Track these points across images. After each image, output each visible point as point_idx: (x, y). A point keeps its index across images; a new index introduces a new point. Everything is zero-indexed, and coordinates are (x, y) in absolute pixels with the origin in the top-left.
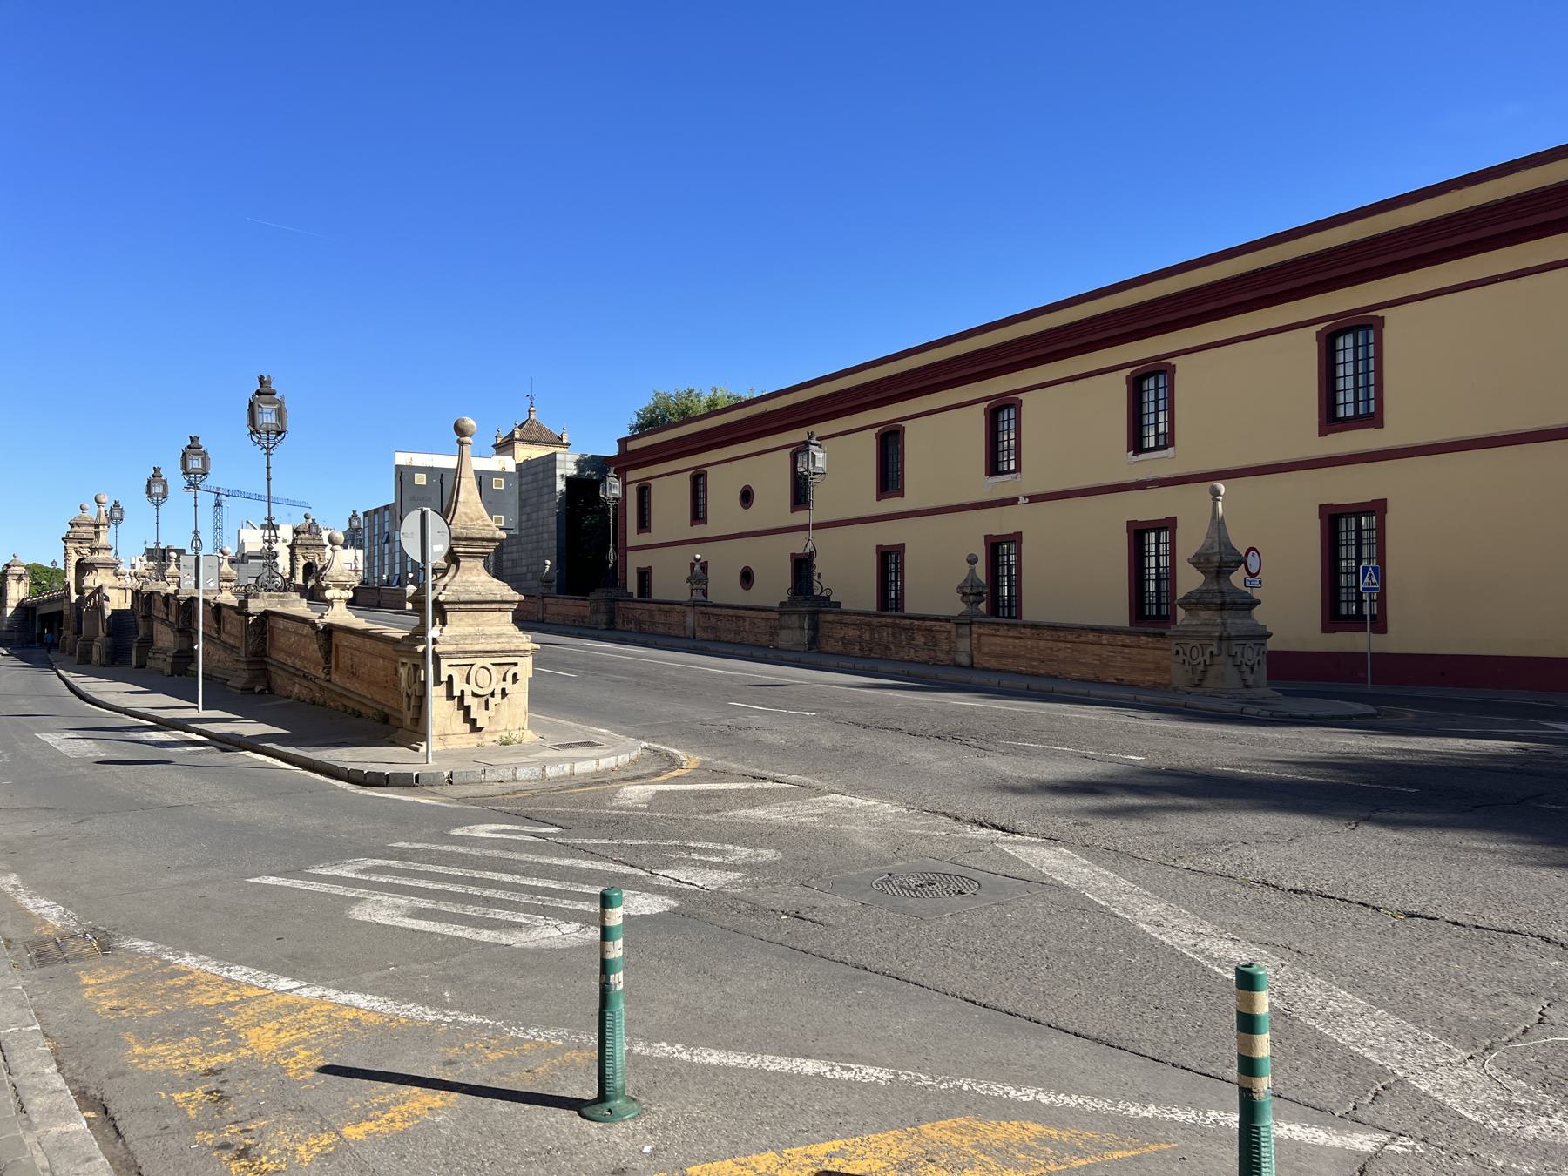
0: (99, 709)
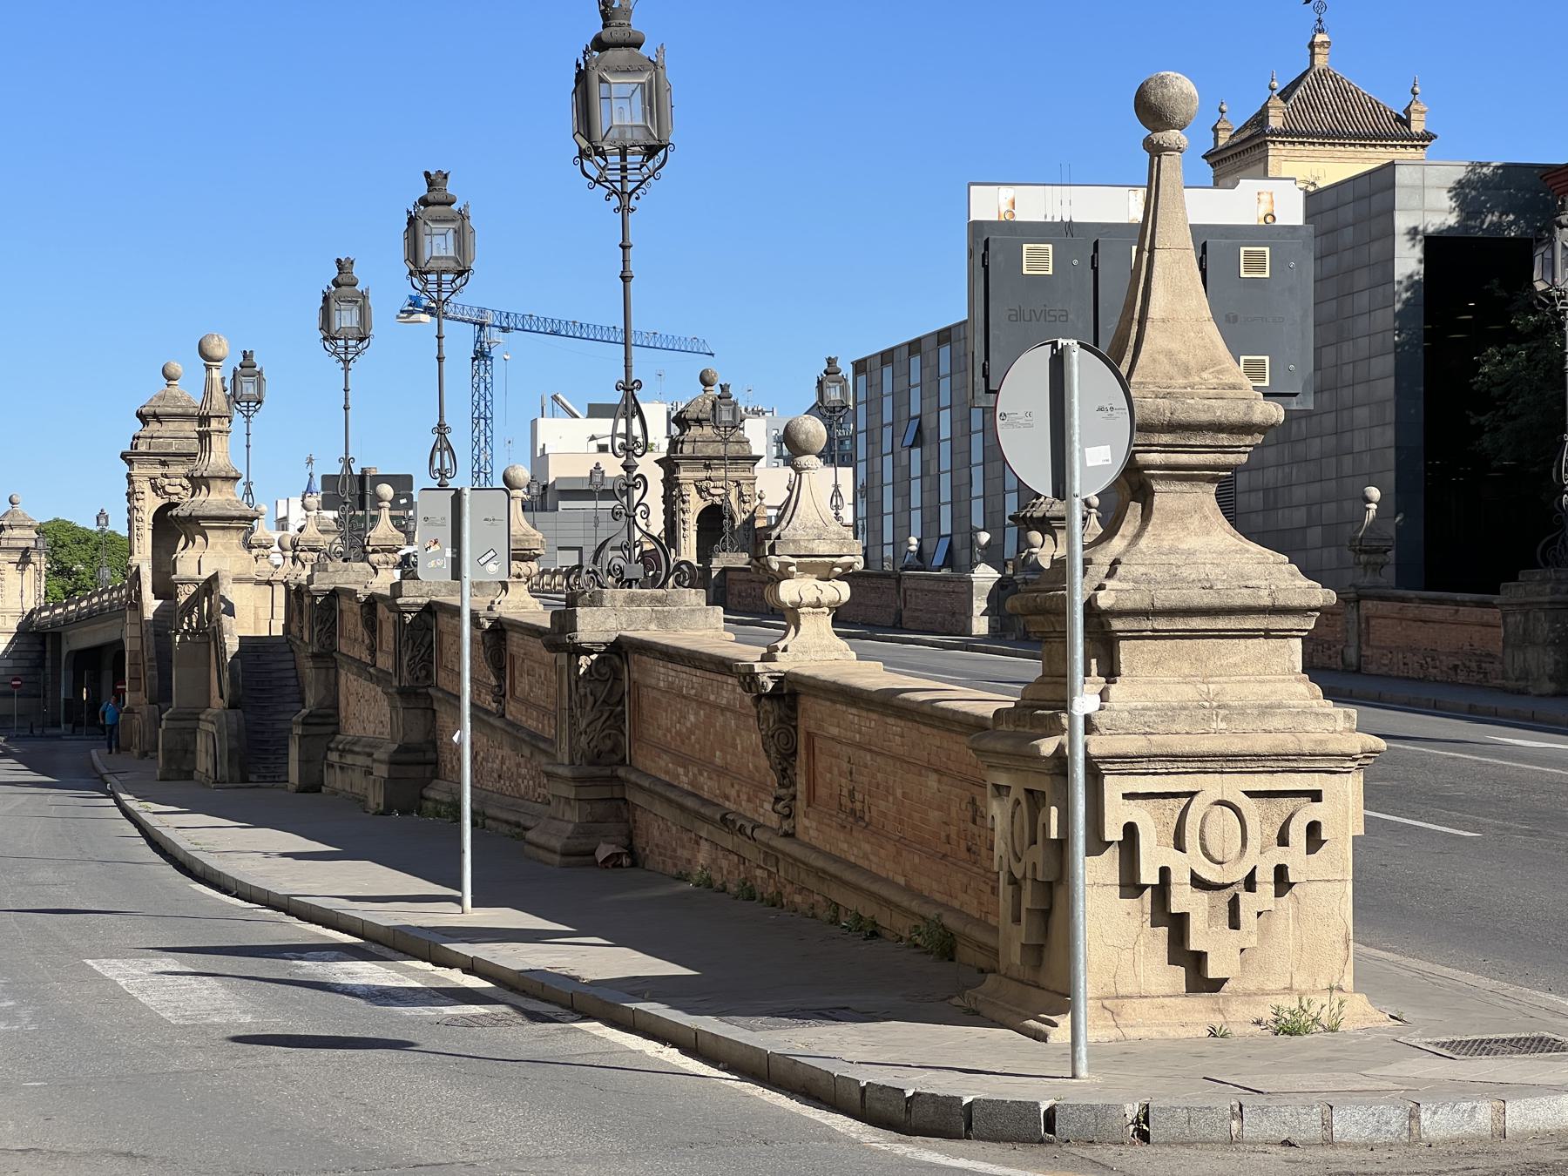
0: (225, 897)
